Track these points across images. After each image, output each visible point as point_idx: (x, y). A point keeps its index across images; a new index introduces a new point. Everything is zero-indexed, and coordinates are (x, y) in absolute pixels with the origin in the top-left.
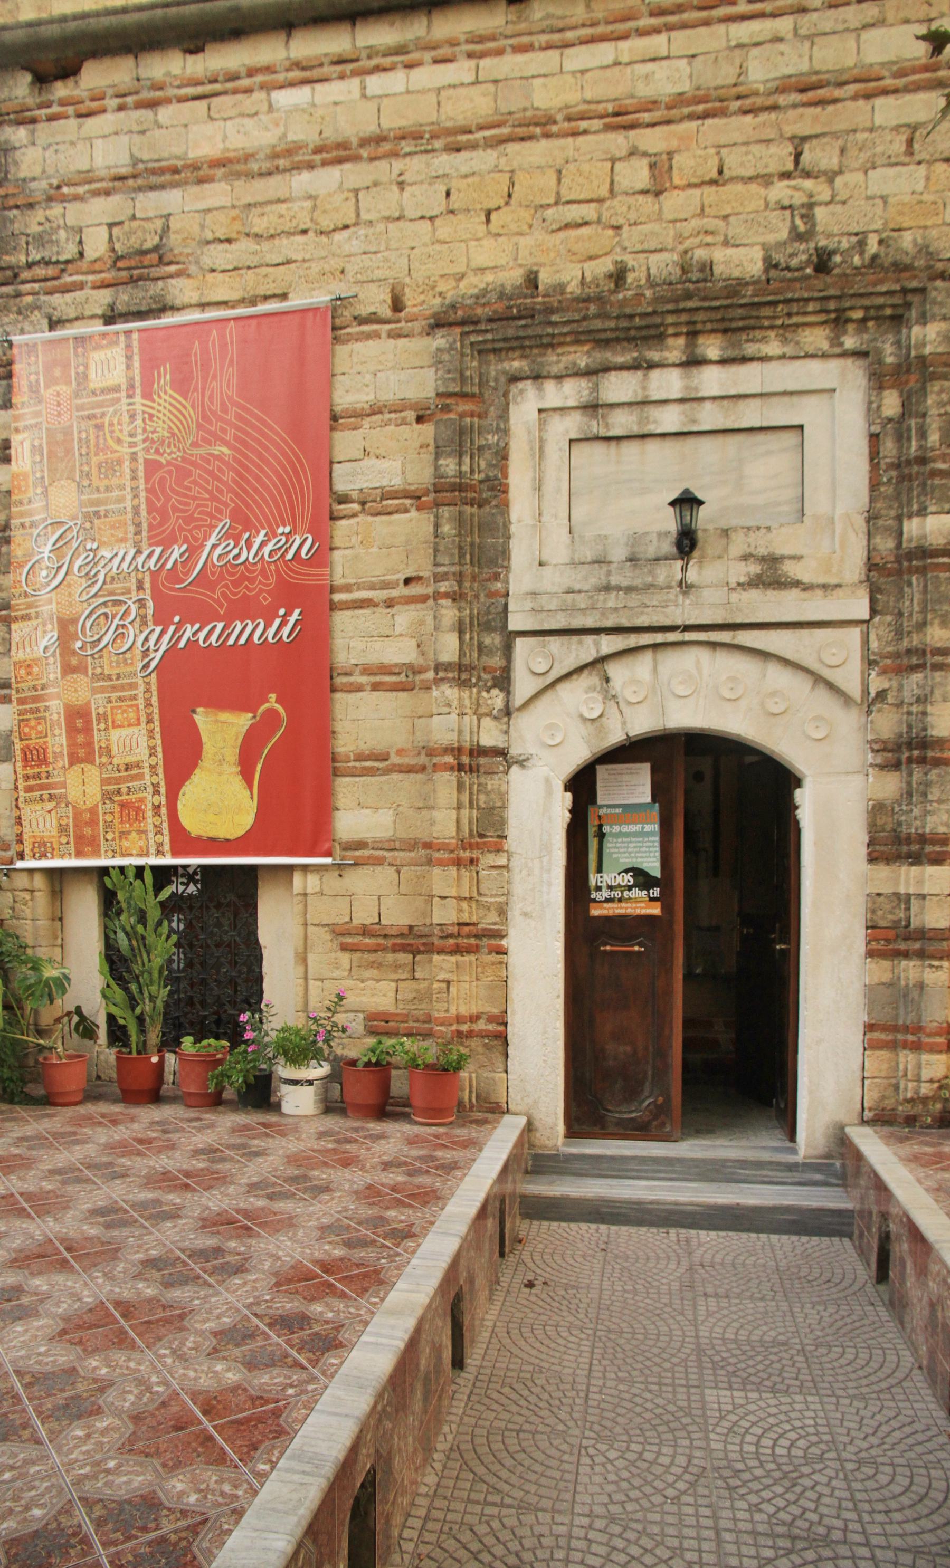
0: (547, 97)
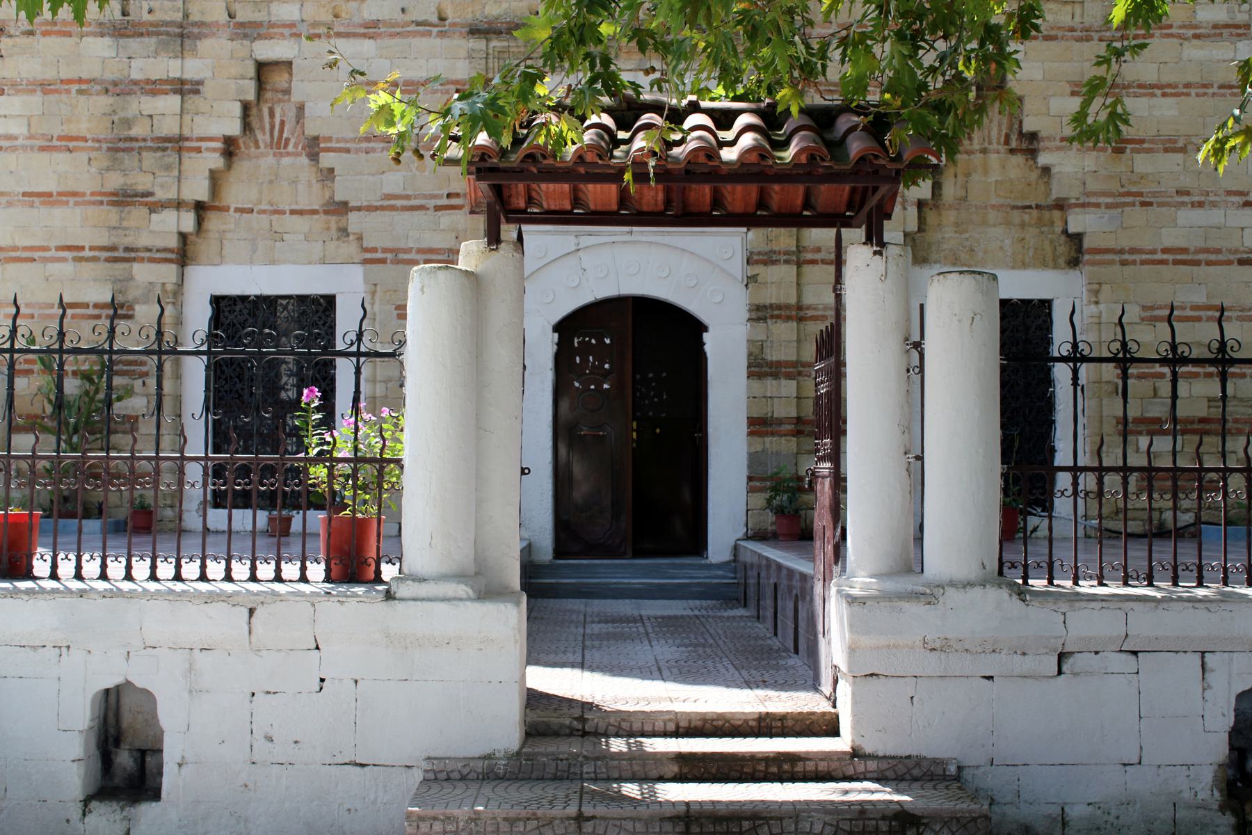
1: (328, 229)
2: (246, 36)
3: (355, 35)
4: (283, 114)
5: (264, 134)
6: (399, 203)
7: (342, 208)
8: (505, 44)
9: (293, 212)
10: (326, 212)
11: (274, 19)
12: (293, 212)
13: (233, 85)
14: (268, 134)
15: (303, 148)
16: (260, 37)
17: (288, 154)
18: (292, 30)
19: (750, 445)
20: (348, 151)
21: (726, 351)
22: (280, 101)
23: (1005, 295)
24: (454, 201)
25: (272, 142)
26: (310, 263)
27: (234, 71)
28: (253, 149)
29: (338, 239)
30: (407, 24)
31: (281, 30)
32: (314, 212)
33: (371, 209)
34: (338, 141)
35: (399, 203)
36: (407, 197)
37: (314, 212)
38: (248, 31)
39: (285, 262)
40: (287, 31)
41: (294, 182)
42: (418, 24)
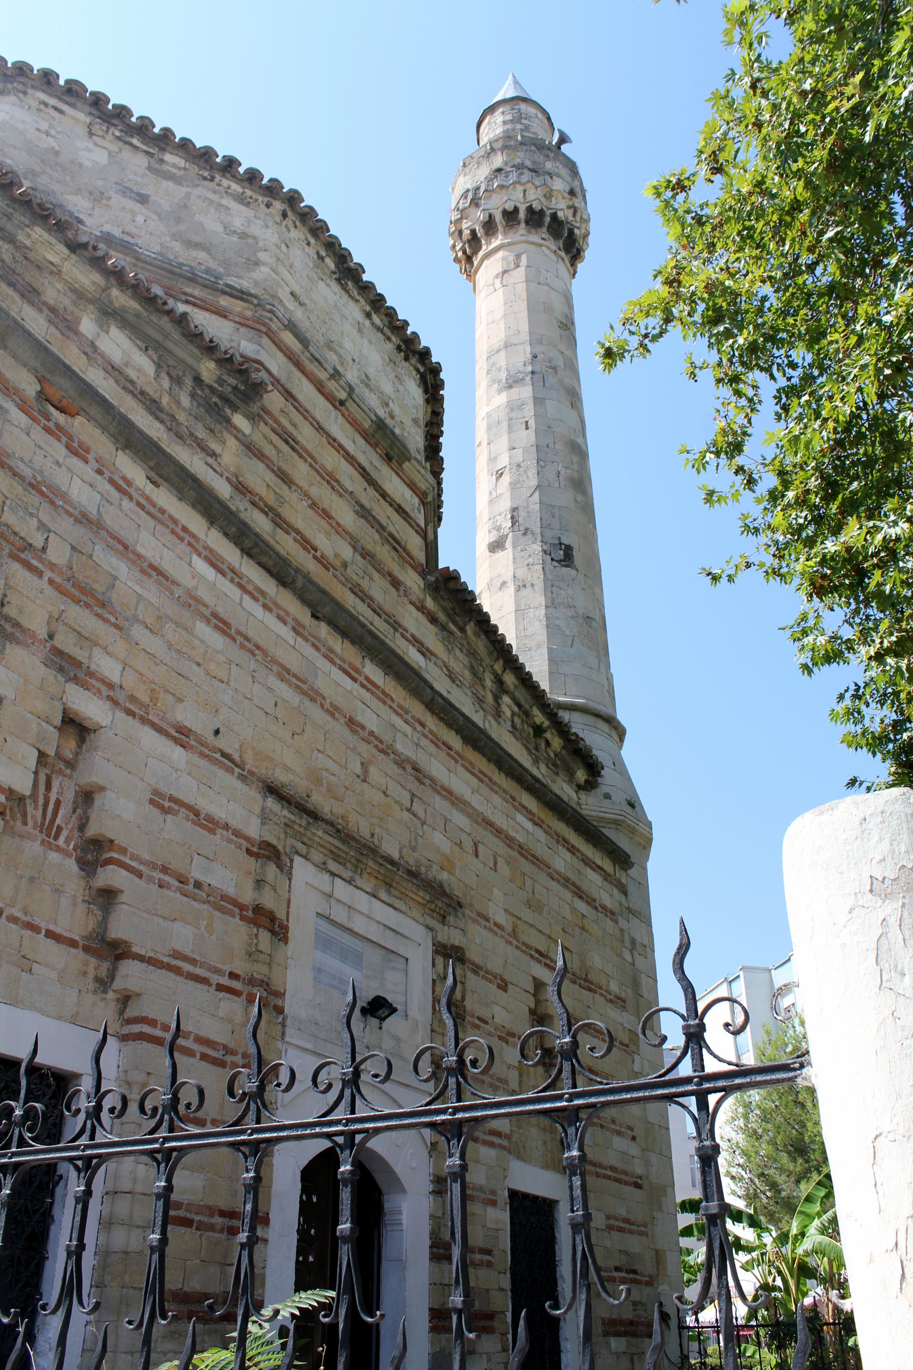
0: (322, 684)
1: (85, 974)
2: (61, 670)
3: (167, 735)
4: (61, 793)
5: (36, 808)
6: (187, 967)
7: (117, 952)
8: (293, 817)
9: (50, 934)
10: (87, 949)
11: (93, 667)
12: (50, 934)
13: (34, 724)
14: (40, 809)
15: (75, 849)
16: (75, 680)
17: (58, 849)
18: (111, 693)
19: (432, 1344)
20: (140, 875)
21: (564, 1216)
22: (60, 772)
23: (561, 1203)
24: (235, 985)
25: (43, 823)
26: (59, 1018)
27: (41, 706)
28: (19, 823)
29: (95, 992)
30: (215, 750)
31: (98, 685)
32: (73, 943)
33: (151, 961)
34: (133, 857)
35: (187, 967)
36: (193, 962)
37: (73, 943)
38: (67, 667)
39: (32, 1007)
40: (105, 691)
41: (58, 891)
42: (224, 755)
